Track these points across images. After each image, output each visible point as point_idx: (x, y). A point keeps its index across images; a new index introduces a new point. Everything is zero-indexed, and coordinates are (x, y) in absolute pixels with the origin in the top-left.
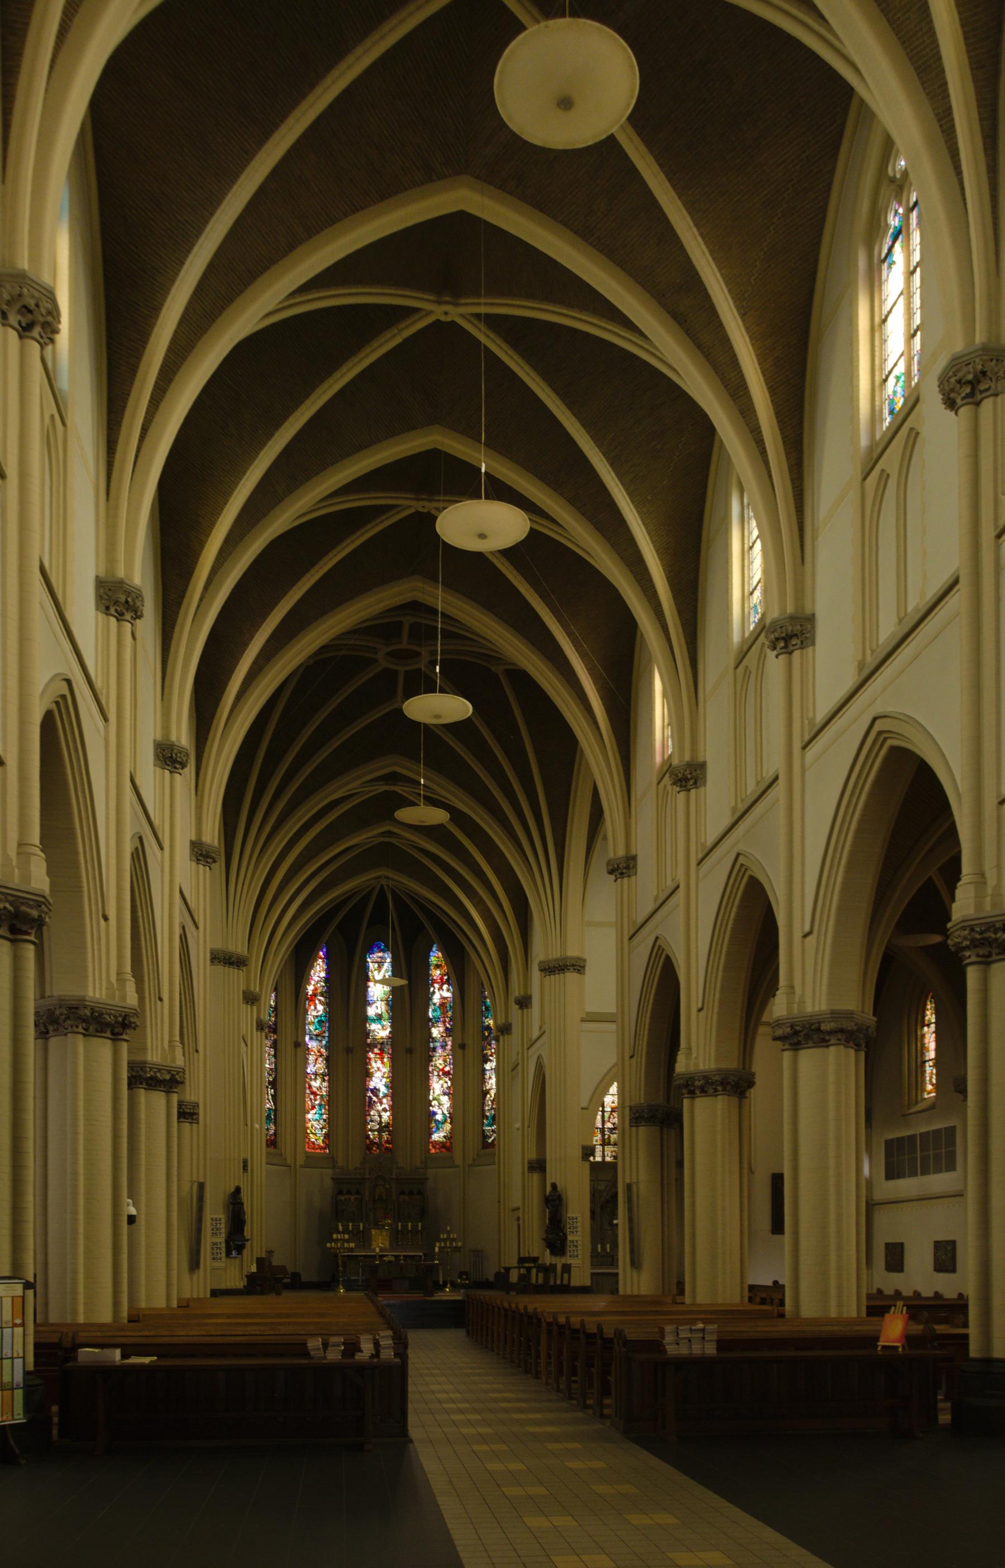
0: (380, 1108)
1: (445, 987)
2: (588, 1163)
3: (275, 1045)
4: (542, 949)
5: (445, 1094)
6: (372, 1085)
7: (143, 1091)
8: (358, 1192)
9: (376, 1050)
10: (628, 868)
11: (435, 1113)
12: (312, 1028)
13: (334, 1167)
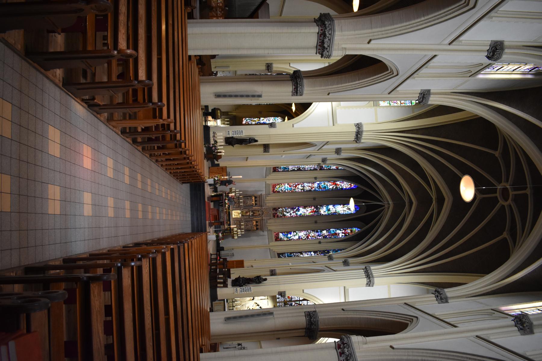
0: (291, 212)
1: (343, 235)
4: (375, 269)
5: (299, 237)
6: (301, 209)
7: (317, 31)
8: (256, 204)
9: (315, 210)
10: (441, 299)
11: (290, 234)
12: (323, 184)
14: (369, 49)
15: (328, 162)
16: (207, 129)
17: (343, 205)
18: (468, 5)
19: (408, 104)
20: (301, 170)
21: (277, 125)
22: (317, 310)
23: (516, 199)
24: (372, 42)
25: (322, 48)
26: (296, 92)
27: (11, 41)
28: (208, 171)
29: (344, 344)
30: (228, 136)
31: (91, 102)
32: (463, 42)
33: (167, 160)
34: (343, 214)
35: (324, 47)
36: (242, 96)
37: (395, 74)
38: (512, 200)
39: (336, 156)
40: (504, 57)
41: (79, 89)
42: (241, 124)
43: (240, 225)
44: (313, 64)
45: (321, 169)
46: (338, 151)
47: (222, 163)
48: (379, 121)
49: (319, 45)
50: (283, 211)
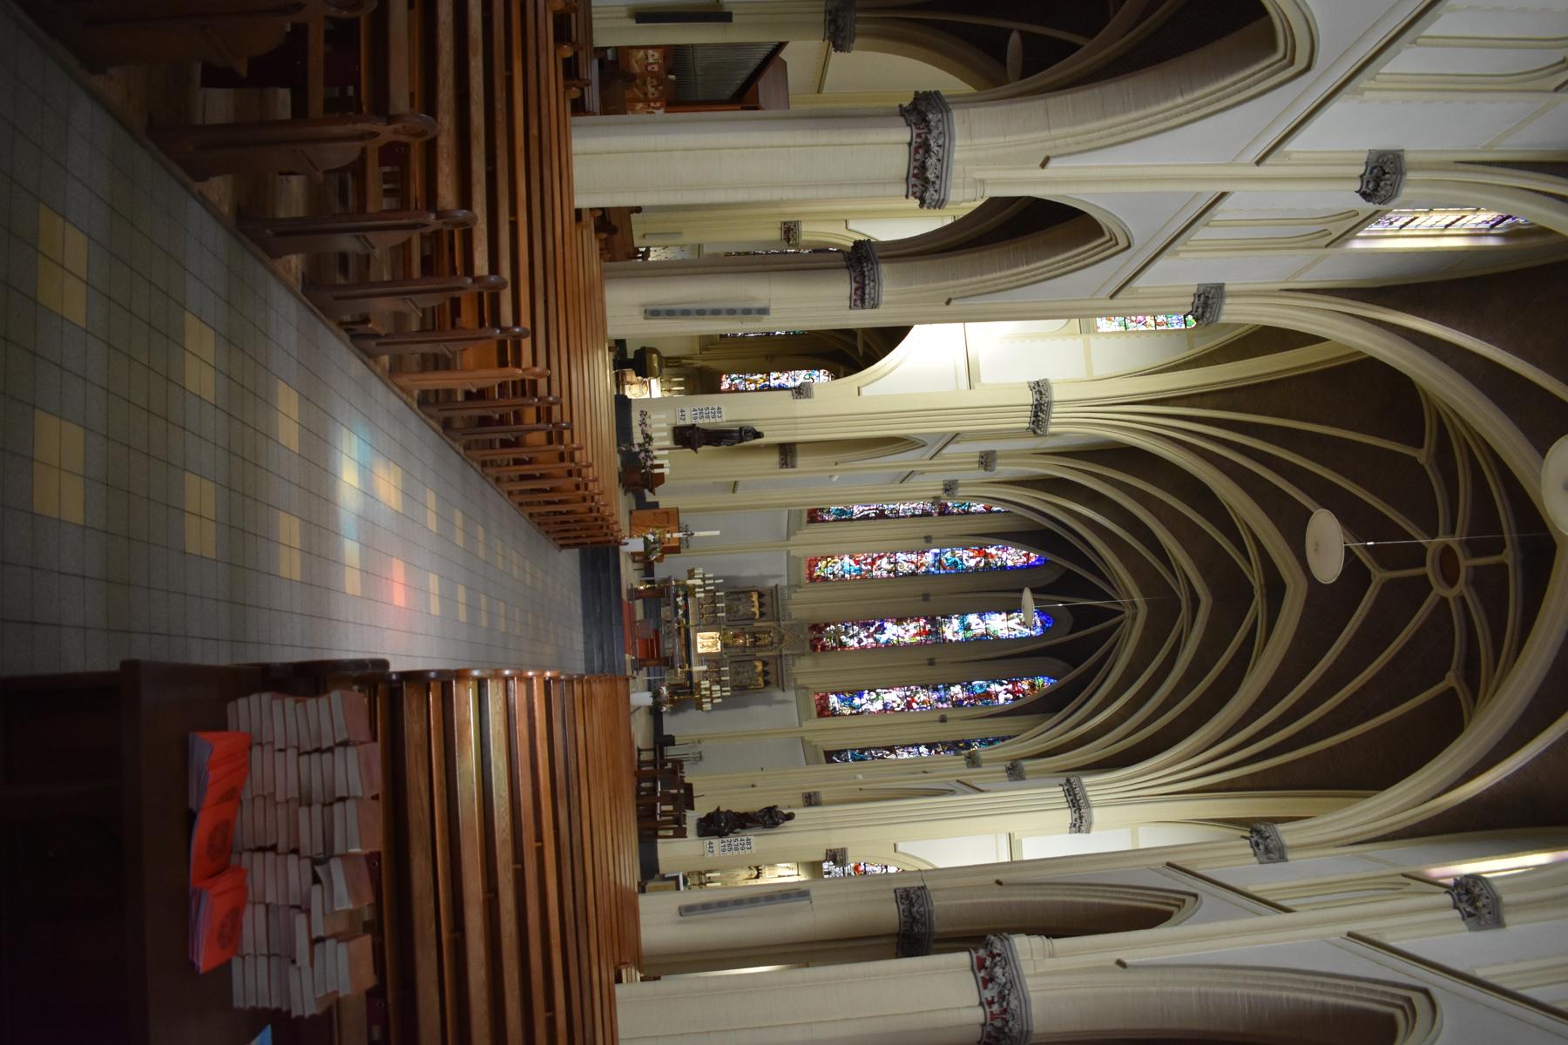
0: (862, 636)
1: (1010, 696)
2: (823, 857)
3: (926, 514)
4: (1093, 786)
6: (888, 625)
7: (908, 138)
8: (762, 614)
10: (1267, 850)
11: (861, 696)
12: (948, 555)
13: (789, 587)
14: (1045, 182)
15: (961, 492)
16: (623, 404)
17: (1009, 613)
18: (1292, 63)
19: (1176, 323)
20: (887, 517)
21: (815, 390)
22: (929, 885)
23: (1479, 579)
24: (1052, 164)
25: (923, 182)
26: (861, 298)
27: (214, 198)
28: (627, 519)
29: (993, 956)
30: (682, 423)
31: (361, 329)
32: (1294, 156)
33: (523, 478)
34: (1008, 640)
35: (926, 180)
36: (716, 312)
37: (1123, 243)
38: (1466, 583)
39: (982, 475)
40: (1406, 192)
41: (337, 298)
42: (714, 388)
43: (719, 673)
44: (908, 223)
45: (941, 514)
46: (987, 460)
47: (663, 498)
48: (1098, 373)
49: (915, 176)
50: (837, 633)
